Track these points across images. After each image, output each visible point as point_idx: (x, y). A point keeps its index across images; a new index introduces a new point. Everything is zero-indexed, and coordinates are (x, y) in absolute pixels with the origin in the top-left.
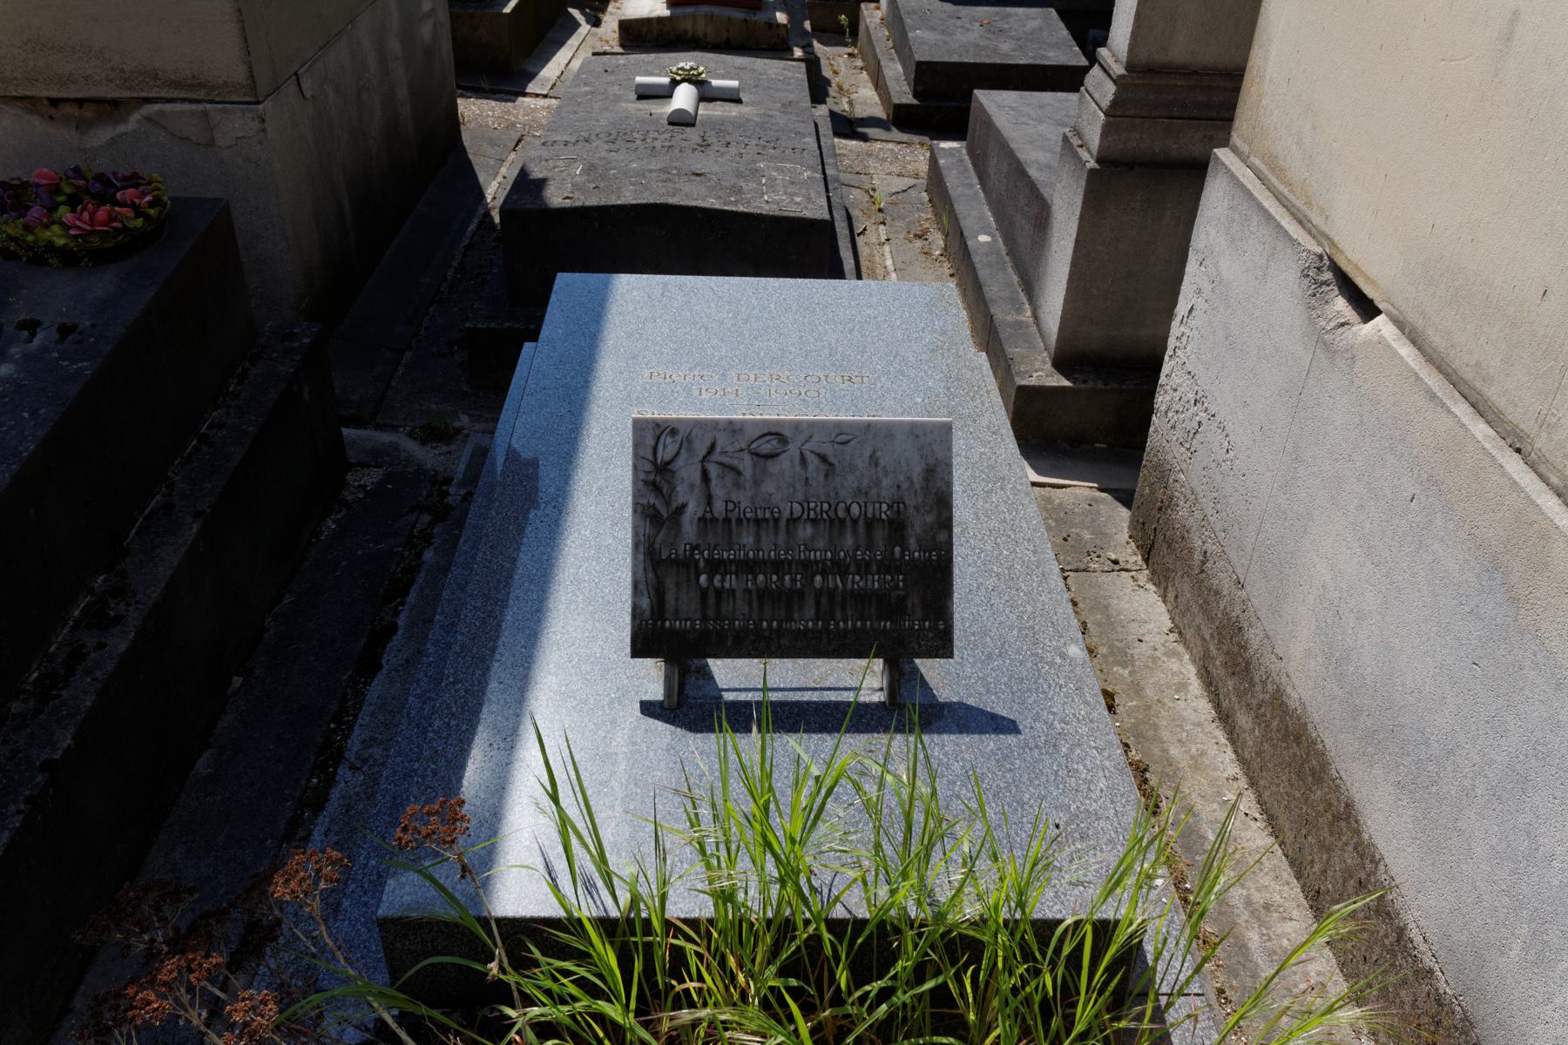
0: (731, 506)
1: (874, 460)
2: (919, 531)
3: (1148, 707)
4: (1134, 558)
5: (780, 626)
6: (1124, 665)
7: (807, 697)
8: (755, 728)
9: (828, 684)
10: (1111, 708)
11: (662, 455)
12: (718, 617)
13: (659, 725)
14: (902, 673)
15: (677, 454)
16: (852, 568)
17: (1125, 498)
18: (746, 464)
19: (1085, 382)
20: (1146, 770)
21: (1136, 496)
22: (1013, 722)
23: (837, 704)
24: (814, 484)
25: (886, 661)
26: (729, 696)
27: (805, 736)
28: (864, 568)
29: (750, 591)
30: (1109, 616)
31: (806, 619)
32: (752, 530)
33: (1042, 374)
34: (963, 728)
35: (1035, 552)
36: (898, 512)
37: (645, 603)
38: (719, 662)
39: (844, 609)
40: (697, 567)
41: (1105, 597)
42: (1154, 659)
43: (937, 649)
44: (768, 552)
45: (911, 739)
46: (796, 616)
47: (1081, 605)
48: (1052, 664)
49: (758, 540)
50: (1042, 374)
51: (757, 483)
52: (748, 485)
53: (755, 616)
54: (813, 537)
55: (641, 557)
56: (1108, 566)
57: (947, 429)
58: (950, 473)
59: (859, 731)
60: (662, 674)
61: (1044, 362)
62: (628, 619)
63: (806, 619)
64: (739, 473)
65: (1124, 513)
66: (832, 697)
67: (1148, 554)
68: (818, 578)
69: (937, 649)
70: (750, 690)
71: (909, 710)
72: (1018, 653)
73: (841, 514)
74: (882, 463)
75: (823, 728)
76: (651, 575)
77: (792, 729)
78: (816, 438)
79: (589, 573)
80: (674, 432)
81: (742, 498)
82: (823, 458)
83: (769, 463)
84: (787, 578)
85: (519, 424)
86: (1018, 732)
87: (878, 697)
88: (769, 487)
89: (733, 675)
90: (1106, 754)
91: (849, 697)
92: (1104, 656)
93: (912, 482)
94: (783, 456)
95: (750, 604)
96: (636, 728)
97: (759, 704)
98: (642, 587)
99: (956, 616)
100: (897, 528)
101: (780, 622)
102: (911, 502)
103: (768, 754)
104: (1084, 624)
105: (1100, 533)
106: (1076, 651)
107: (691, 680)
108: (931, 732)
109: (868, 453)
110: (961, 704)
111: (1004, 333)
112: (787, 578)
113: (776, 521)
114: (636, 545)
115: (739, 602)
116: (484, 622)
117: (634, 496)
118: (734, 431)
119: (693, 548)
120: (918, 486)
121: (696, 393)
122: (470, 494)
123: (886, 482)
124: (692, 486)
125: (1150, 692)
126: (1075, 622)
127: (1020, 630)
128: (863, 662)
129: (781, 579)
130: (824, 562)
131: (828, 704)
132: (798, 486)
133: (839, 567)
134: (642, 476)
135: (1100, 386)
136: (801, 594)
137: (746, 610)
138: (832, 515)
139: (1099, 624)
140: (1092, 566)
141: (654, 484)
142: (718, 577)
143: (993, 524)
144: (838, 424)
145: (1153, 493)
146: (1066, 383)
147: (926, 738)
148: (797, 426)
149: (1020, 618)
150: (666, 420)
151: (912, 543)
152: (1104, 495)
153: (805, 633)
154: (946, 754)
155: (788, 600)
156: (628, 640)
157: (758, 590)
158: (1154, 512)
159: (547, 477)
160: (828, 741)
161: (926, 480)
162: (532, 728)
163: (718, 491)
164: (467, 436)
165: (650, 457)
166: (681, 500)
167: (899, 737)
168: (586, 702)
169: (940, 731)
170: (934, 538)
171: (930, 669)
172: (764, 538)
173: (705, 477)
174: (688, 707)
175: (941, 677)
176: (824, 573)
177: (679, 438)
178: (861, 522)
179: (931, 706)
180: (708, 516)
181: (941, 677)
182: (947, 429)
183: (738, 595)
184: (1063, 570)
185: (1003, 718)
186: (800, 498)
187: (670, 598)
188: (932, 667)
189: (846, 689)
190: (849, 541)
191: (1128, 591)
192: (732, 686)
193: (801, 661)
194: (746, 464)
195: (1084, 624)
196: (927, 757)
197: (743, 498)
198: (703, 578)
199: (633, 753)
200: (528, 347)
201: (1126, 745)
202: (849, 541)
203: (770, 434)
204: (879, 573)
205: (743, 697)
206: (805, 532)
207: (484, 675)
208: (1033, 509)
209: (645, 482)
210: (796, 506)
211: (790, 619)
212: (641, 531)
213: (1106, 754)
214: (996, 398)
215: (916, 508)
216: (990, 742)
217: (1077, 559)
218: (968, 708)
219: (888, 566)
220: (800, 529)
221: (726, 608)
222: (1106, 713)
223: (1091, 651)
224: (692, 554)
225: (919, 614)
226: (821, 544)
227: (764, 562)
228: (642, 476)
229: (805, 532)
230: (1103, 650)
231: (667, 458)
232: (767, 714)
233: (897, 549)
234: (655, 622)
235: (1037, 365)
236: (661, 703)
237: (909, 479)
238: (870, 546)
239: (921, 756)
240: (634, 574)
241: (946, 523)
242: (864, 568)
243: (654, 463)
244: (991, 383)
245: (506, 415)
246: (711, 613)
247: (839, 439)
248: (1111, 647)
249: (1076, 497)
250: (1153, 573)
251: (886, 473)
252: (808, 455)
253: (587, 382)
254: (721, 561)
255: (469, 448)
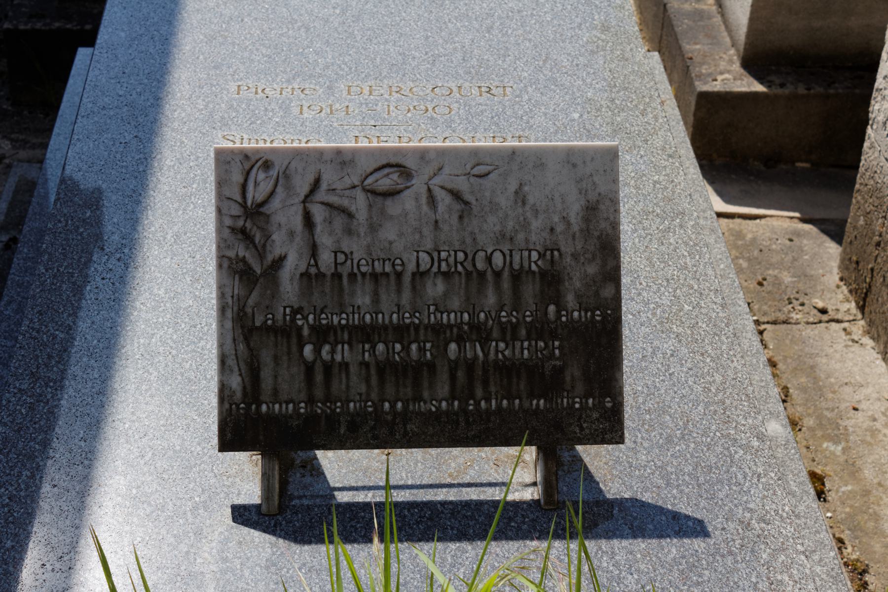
0: (341, 258)
1: (520, 197)
2: (578, 284)
3: (866, 493)
4: (843, 303)
5: (406, 408)
6: (836, 440)
7: (441, 495)
8: (376, 540)
9: (467, 479)
10: (820, 495)
11: (255, 199)
12: (328, 398)
13: (256, 535)
14: (559, 464)
15: (272, 193)
16: (495, 334)
17: (835, 230)
18: (359, 204)
19: (782, 85)
20: (865, 571)
21: (848, 227)
22: (700, 522)
23: (480, 504)
24: (445, 228)
25: (539, 449)
26: (343, 497)
27: (440, 546)
28: (510, 333)
29: (367, 365)
30: (816, 379)
31: (438, 398)
32: (369, 286)
33: (730, 77)
34: (637, 531)
35: (723, 306)
36: (552, 261)
37: (235, 382)
38: (330, 453)
39: (486, 383)
40: (300, 336)
41: (811, 356)
42: (873, 432)
43: (604, 432)
44: (389, 316)
45: (574, 545)
46: (426, 394)
47: (781, 366)
48: (747, 448)
49: (376, 300)
50: (730, 77)
51: (373, 228)
52: (362, 231)
53: (374, 396)
54: (446, 295)
55: (229, 324)
56: (815, 316)
57: (612, 155)
58: (617, 211)
59: (509, 538)
60: (258, 470)
61: (731, 62)
62: (214, 401)
63: (438, 398)
64: (350, 216)
65: (833, 249)
66: (473, 494)
67: (863, 299)
68: (453, 346)
69: (604, 432)
70: (370, 488)
71: (570, 510)
72: (705, 434)
73: (480, 265)
74: (531, 200)
75: (462, 536)
76: (241, 347)
77: (425, 537)
78: (446, 170)
79: (164, 343)
80: (267, 165)
81: (355, 248)
82: (456, 195)
83: (389, 202)
84: (414, 347)
85: (75, 147)
86: (705, 534)
87: (529, 495)
88: (389, 233)
89: (346, 470)
90: (816, 557)
91: (495, 494)
92: (811, 429)
93: (569, 224)
94: (407, 193)
95: (367, 380)
96: (227, 540)
97: (380, 506)
98: (231, 362)
99: (627, 389)
100: (551, 280)
101: (406, 403)
102: (567, 248)
103: (394, 568)
104: (785, 390)
105: (804, 276)
106: (776, 428)
107: (295, 478)
108: (597, 537)
109: (513, 187)
110: (634, 501)
111: (682, 25)
112: (414, 347)
113: (399, 275)
114: (222, 310)
115: (354, 379)
116: (32, 408)
117: (219, 247)
118: (343, 163)
119: (296, 311)
120: (576, 228)
121: (296, 111)
122: (14, 240)
123: (535, 224)
124: (291, 234)
125: (868, 473)
126: (775, 391)
127: (707, 405)
128: (513, 451)
129: (406, 348)
130: (459, 326)
131: (467, 504)
132: (426, 231)
133: (479, 332)
134: (228, 222)
135: (801, 90)
136: (432, 367)
137: (363, 388)
138: (470, 268)
139: (803, 389)
140: (795, 316)
141: (243, 231)
142: (327, 348)
143: (671, 271)
144: (475, 152)
145: (868, 224)
146: (758, 87)
147: (590, 545)
148: (423, 154)
149: (707, 390)
150: (257, 151)
151: (570, 300)
152: (808, 227)
153: (438, 416)
154: (616, 565)
155: (417, 373)
156: (215, 428)
157: (377, 363)
158: (871, 248)
159: (112, 219)
160: (470, 550)
161: (587, 220)
162: (91, 541)
163: (325, 240)
164: (9, 166)
165: (239, 198)
166: (277, 252)
167: (557, 544)
168: (163, 508)
169: (609, 535)
170: (597, 294)
171: (596, 457)
172: (384, 297)
173: (308, 221)
174: (292, 511)
175: (609, 468)
176: (460, 340)
177: (274, 173)
178: (506, 274)
179: (598, 503)
180: (313, 270)
181: (609, 468)
182: (612, 155)
183: (353, 369)
184: (757, 323)
185: (688, 517)
186: (429, 246)
187: (266, 374)
188: (597, 455)
189: (490, 485)
190: (491, 299)
191: (839, 347)
192: (346, 483)
193: (433, 451)
194: (359, 204)
195: (785, 390)
196: (592, 569)
197: (357, 247)
198: (308, 350)
199: (224, 572)
200: (83, 54)
201: (840, 541)
202: (491, 299)
203: (389, 165)
204: (529, 338)
205: (361, 497)
206: (436, 288)
207: (33, 476)
208: (720, 249)
209: (233, 229)
210: (423, 255)
211: (418, 398)
212: (228, 291)
213: (816, 557)
214: (673, 111)
215: (575, 256)
216: (672, 548)
217: (775, 308)
218: (644, 505)
219: (540, 330)
220: (429, 284)
221: (338, 386)
222: (815, 504)
223: (794, 424)
224: (293, 320)
225: (580, 388)
226: (456, 303)
227: (385, 328)
228: (228, 222)
229: (436, 288)
230: (809, 422)
231: (260, 198)
232: (391, 519)
233: (552, 308)
234: (248, 406)
235: (723, 65)
236: (258, 507)
237: (565, 219)
238: (517, 305)
239: (586, 568)
240: (221, 346)
241: (613, 276)
242: (510, 333)
243: (244, 205)
244: (667, 91)
245: (57, 141)
246: (319, 393)
247: (476, 171)
248: (820, 417)
249: (773, 231)
250: (871, 323)
251: (536, 212)
252: (437, 191)
253: (158, 99)
254: (330, 328)
255: (12, 182)
